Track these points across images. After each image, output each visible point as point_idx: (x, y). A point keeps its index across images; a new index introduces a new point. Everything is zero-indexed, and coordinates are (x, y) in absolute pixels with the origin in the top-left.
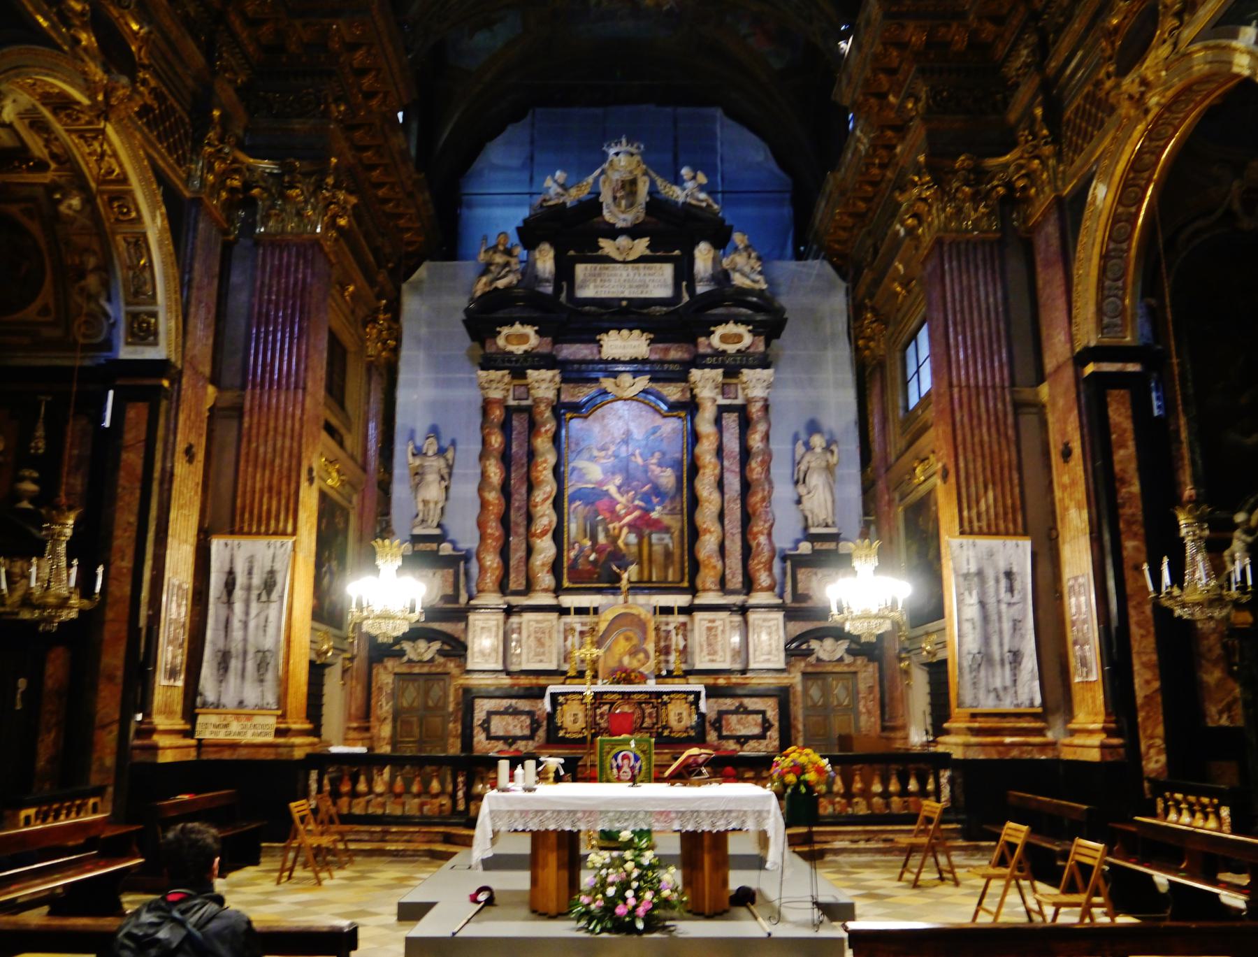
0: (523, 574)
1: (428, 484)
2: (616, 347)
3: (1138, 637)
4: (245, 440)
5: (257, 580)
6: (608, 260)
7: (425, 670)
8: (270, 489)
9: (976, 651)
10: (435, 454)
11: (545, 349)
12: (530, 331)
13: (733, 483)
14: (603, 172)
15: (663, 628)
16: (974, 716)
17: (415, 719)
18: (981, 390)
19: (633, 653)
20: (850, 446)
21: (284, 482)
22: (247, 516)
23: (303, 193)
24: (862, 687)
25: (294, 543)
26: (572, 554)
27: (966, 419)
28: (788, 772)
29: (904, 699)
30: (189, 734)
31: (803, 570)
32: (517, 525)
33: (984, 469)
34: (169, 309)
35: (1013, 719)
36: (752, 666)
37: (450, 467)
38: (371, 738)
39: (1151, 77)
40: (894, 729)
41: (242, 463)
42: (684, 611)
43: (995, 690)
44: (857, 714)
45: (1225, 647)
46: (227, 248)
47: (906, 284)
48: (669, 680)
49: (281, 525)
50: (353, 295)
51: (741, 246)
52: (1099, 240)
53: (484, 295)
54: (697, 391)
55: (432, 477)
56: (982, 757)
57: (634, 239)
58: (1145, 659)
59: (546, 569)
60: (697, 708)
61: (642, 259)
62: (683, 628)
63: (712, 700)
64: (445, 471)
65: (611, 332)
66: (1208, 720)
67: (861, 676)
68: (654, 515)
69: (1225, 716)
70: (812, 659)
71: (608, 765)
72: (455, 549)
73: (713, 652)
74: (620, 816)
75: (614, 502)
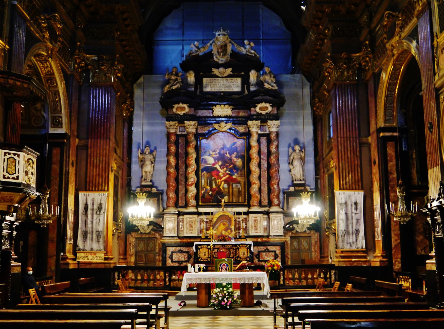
0: (184, 200)
1: (147, 165)
2: (219, 111)
3: (393, 226)
4: (89, 158)
5: (95, 207)
6: (217, 76)
7: (147, 236)
8: (99, 175)
9: (343, 230)
10: (149, 153)
11: (192, 113)
12: (185, 106)
13: (265, 164)
14: (214, 42)
15: (238, 220)
16: (342, 252)
17: (143, 255)
18: (348, 139)
19: (226, 230)
20: (310, 149)
21: (104, 172)
22: (91, 184)
23: (106, 68)
24: (313, 242)
25: (108, 194)
26: (203, 192)
27: (343, 149)
28: (269, 267)
29: (327, 246)
30: (75, 259)
31: (291, 198)
32: (181, 181)
33: (348, 166)
34: (66, 116)
35: (356, 253)
36: (271, 234)
37: (154, 158)
38: (127, 262)
39: (394, 45)
40: (324, 257)
41: (89, 166)
42: (245, 213)
43: (350, 243)
44: (311, 252)
45: (424, 228)
46: (80, 87)
47: (328, 91)
48: (240, 240)
49: (103, 188)
50: (119, 96)
51: (268, 72)
52: (384, 91)
53: (168, 92)
54: (250, 129)
55: (148, 163)
56: (344, 265)
57: (226, 69)
58: (395, 232)
59: (193, 198)
60: (250, 250)
61: (229, 76)
62: (245, 220)
63: (256, 247)
64: (153, 160)
65: (217, 106)
66: (418, 253)
67: (313, 237)
68: (234, 177)
69: (423, 252)
70: (294, 231)
71: (218, 268)
72: (157, 190)
73: (256, 229)
74: (223, 279)
75: (219, 172)
